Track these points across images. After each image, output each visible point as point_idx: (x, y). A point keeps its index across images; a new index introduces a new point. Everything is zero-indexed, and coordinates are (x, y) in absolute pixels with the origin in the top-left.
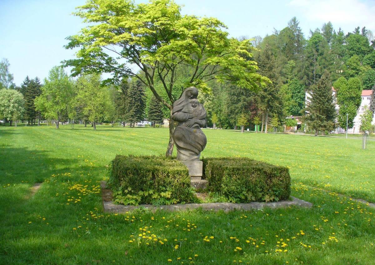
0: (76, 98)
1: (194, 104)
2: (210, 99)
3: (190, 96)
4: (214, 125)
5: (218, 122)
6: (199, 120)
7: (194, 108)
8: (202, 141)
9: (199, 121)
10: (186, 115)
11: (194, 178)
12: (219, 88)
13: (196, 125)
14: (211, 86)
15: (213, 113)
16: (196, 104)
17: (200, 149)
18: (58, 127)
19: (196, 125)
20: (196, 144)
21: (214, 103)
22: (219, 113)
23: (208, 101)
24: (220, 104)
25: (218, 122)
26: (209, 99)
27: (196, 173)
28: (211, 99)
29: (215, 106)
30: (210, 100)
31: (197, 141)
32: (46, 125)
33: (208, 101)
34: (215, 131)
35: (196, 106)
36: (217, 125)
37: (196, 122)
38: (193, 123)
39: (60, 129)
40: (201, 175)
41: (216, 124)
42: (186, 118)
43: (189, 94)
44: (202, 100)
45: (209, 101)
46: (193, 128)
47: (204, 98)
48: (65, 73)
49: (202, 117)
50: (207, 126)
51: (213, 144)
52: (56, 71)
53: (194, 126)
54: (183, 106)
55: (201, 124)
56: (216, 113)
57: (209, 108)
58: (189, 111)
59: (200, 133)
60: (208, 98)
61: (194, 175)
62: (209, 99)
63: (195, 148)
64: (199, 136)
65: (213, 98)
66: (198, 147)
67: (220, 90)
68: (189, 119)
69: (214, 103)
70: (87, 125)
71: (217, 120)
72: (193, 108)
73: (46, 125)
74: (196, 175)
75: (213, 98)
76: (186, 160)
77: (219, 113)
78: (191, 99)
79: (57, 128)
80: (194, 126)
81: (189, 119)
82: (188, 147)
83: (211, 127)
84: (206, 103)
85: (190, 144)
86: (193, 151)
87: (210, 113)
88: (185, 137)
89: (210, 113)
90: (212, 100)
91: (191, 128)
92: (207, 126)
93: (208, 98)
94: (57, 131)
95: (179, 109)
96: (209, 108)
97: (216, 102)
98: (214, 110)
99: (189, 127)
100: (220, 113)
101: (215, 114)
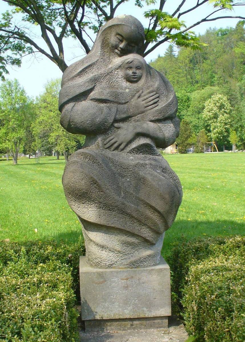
0: (38, 121)
1: (130, 72)
2: (226, 111)
3: (116, 47)
4: (234, 147)
5: (239, 142)
6: (152, 124)
7: (135, 85)
8: (163, 198)
9: (151, 127)
10: (105, 110)
11: (144, 322)
12: (238, 95)
13: (143, 141)
14: (227, 94)
15: (231, 130)
16: (138, 72)
17: (155, 224)
18: (16, 162)
19: (143, 141)
20: (142, 208)
21: (231, 116)
22: (239, 129)
23: (223, 115)
24: (240, 118)
25: (239, 142)
26: (225, 112)
27: (150, 306)
28: (228, 111)
29: (233, 121)
30: (227, 113)
31: (142, 195)
32: (6, 160)
33: (223, 115)
34: (235, 154)
35: (139, 78)
36: (238, 147)
37: (139, 130)
38: (130, 136)
39: (18, 165)
40: (167, 311)
41: (236, 145)
42: (105, 121)
43: (113, 39)
44: (216, 114)
45: (225, 115)
46: (132, 151)
47: (218, 110)
48: (20, 88)
49: (161, 111)
50: (224, 148)
51: (231, 175)
52: (8, 86)
53: (134, 145)
54: (95, 80)
55: (160, 135)
56: (236, 130)
57: (226, 124)
58: (116, 95)
59: (154, 167)
60: (223, 110)
61: (142, 316)
62: (225, 112)
63: (140, 221)
64: (149, 178)
65: (231, 110)
66: (147, 218)
67: (239, 98)
68: (116, 121)
69: (231, 116)
70: (60, 157)
71: (237, 140)
72: (128, 84)
73: (6, 160)
74: (148, 315)
75: (231, 110)
76: (110, 266)
77: (239, 129)
78: (120, 56)
79: (15, 164)
80: (134, 145)
81: (116, 121)
82: (115, 221)
83: (229, 150)
84: (221, 118)
85: (123, 212)
86: (133, 235)
87: (227, 131)
88: (99, 187)
89: (227, 131)
90: (229, 113)
91: (124, 154)
92: (224, 148)
93: (223, 110)
94: (14, 169)
95: (78, 91)
96: (226, 124)
97: (234, 115)
98: (233, 126)
99: (117, 148)
100: (241, 130)
101: (234, 132)
